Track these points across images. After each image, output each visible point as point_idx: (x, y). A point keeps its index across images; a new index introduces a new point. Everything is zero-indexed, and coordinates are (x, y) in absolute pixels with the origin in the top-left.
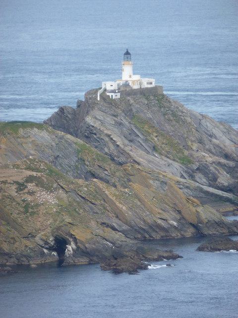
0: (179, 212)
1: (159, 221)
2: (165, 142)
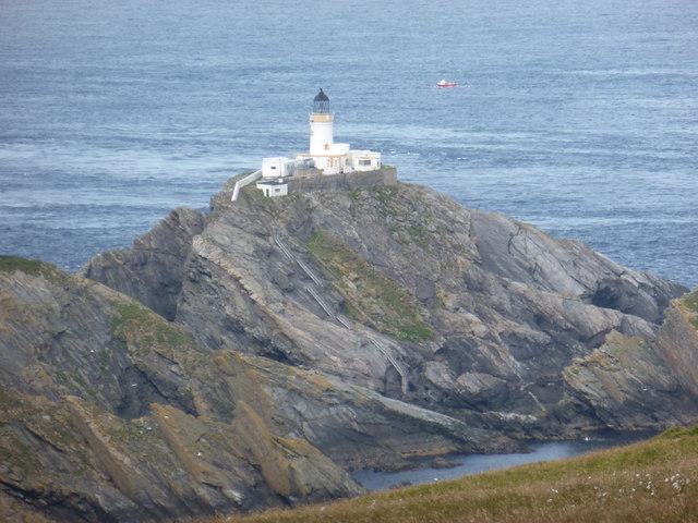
1: (203, 492)
2: (373, 290)
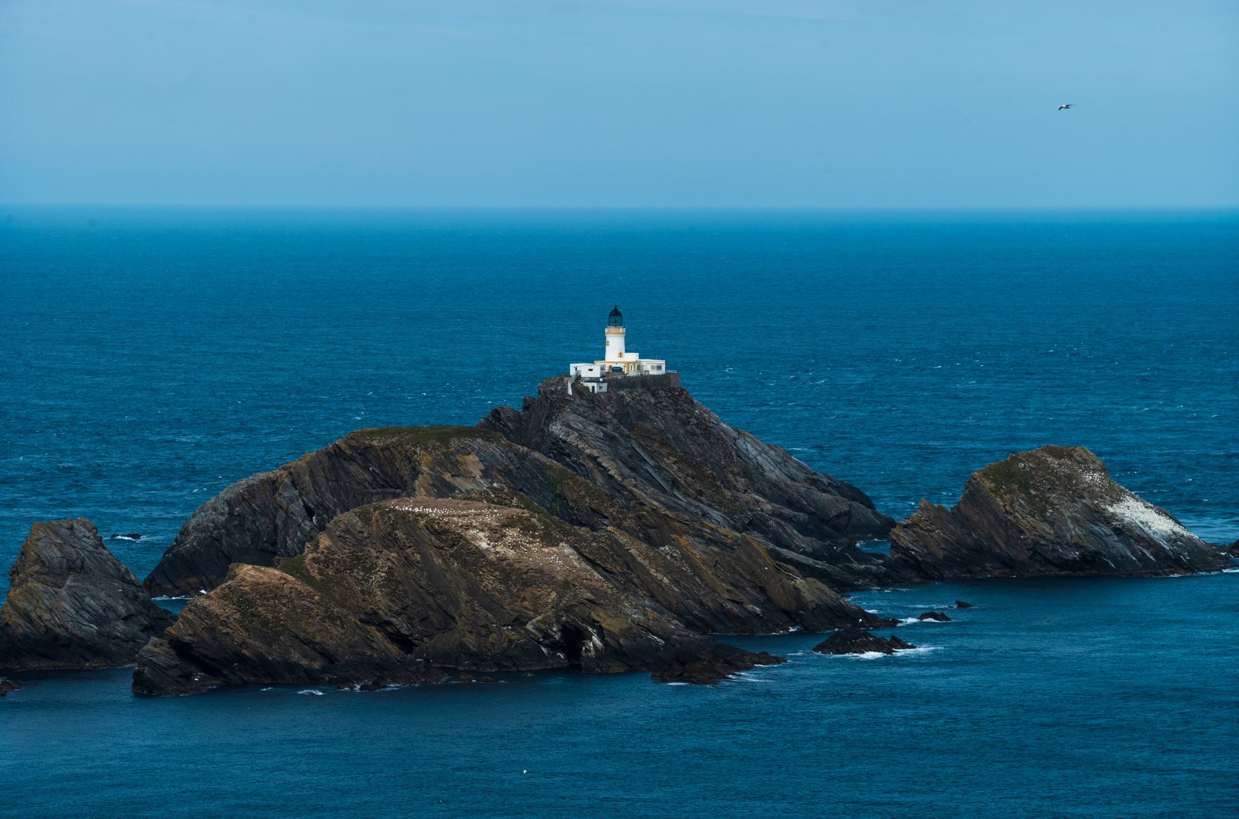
0: (763, 590)
1: (729, 606)
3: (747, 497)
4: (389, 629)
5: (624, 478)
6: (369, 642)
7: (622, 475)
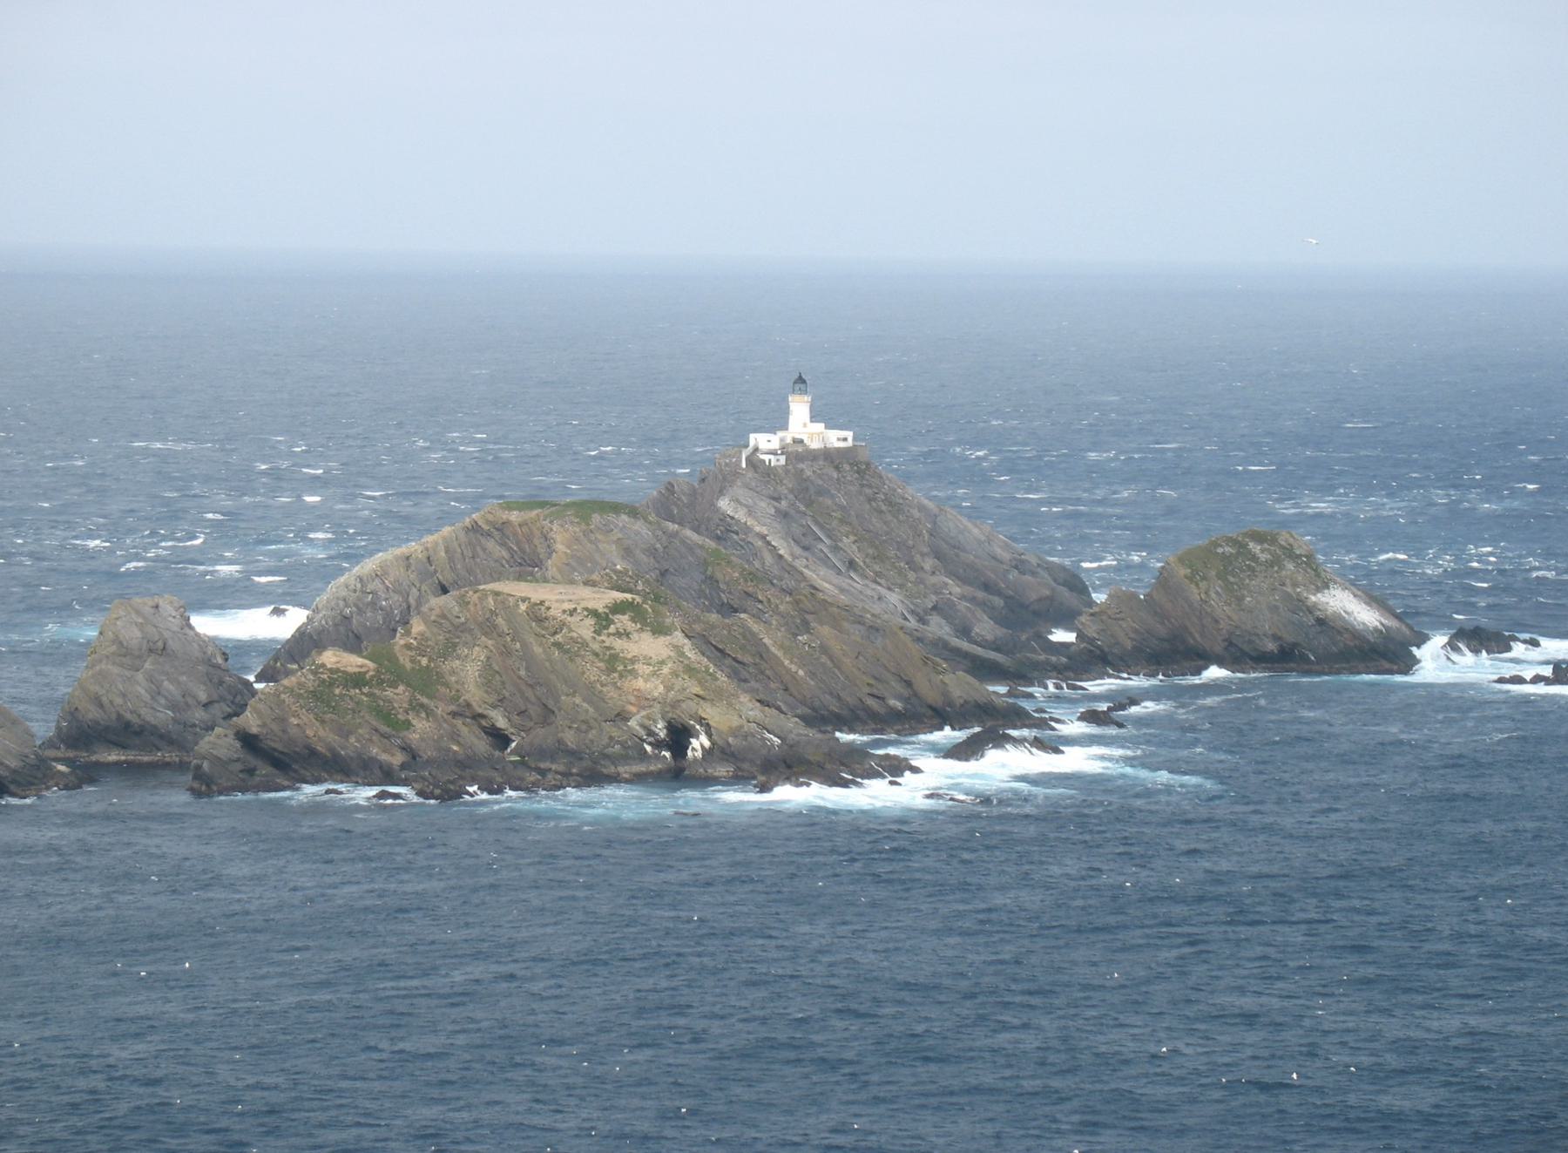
1: (870, 702)
3: (933, 580)
4: (484, 723)
5: (795, 557)
6: (455, 736)
7: (792, 554)
